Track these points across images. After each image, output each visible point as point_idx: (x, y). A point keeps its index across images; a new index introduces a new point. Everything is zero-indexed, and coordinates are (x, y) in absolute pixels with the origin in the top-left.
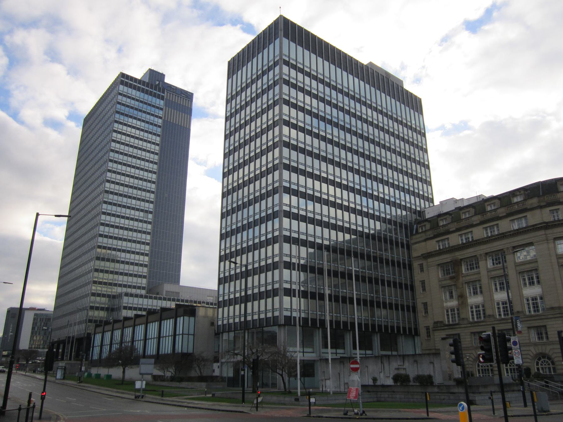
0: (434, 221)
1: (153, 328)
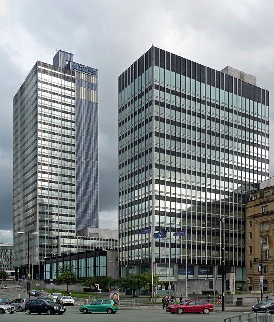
1: (82, 262)
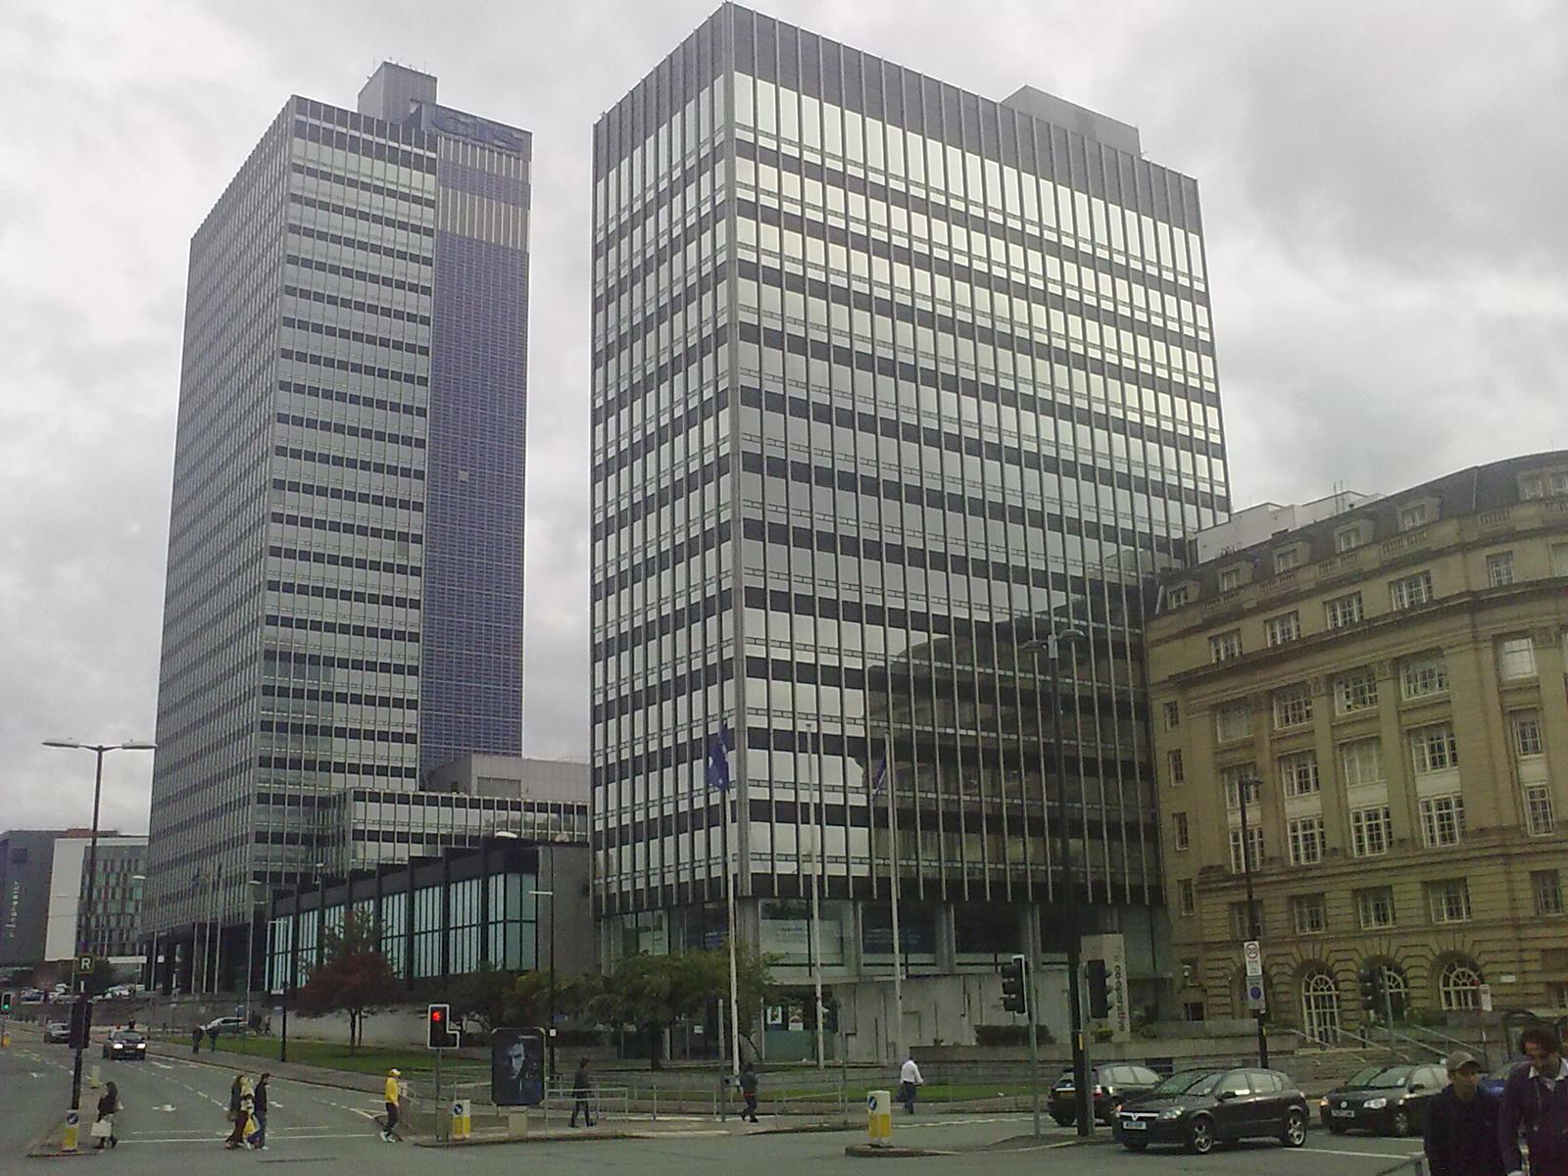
0: (1259, 560)
1: (429, 901)
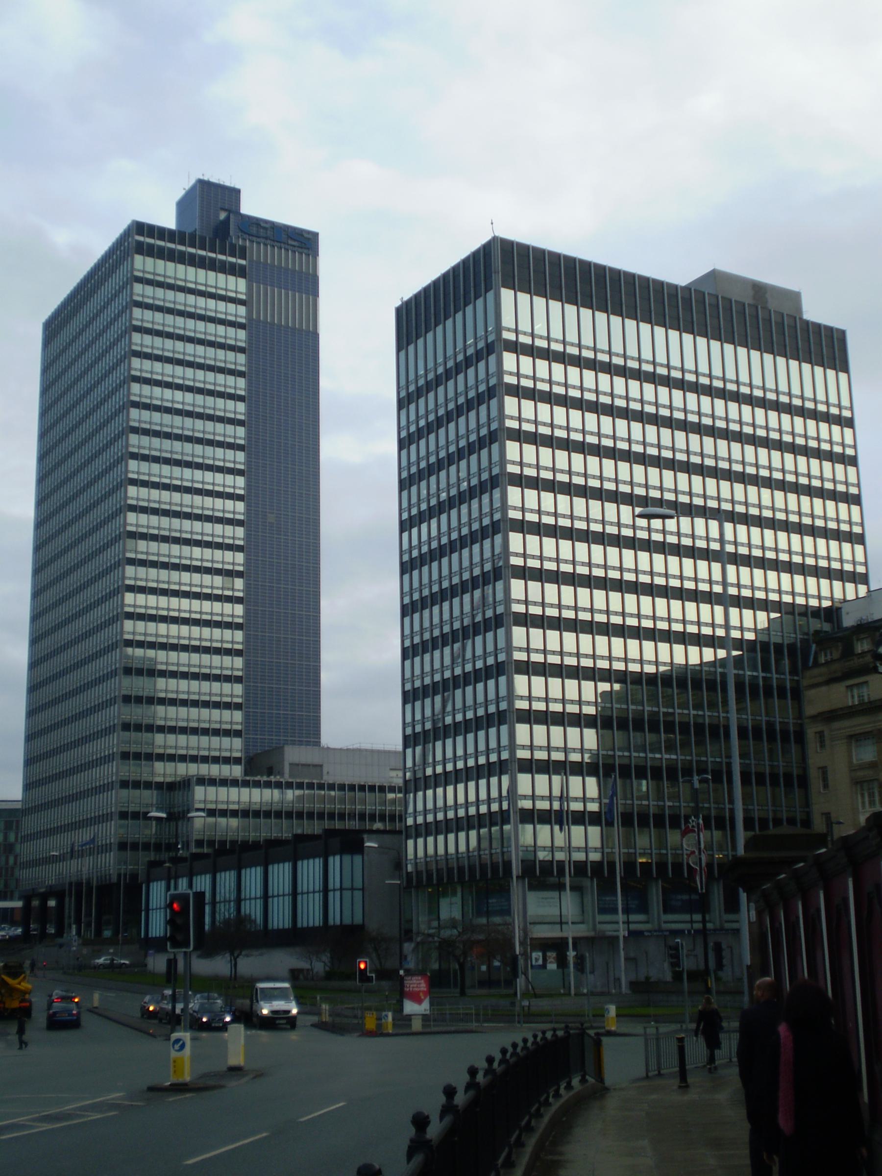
1: (280, 873)
